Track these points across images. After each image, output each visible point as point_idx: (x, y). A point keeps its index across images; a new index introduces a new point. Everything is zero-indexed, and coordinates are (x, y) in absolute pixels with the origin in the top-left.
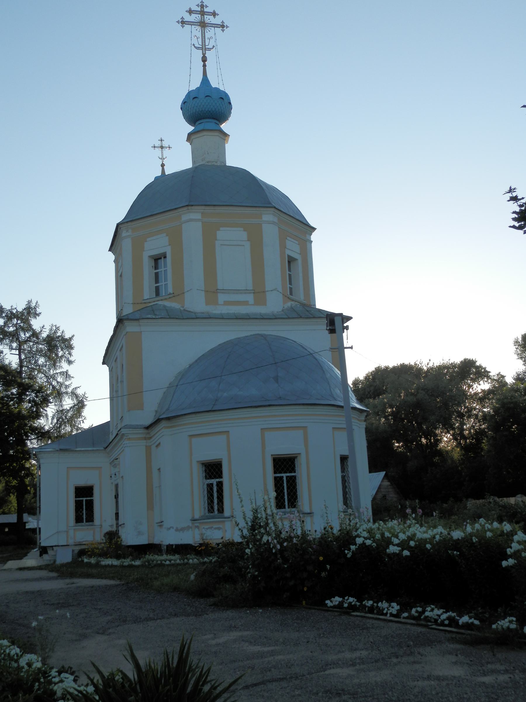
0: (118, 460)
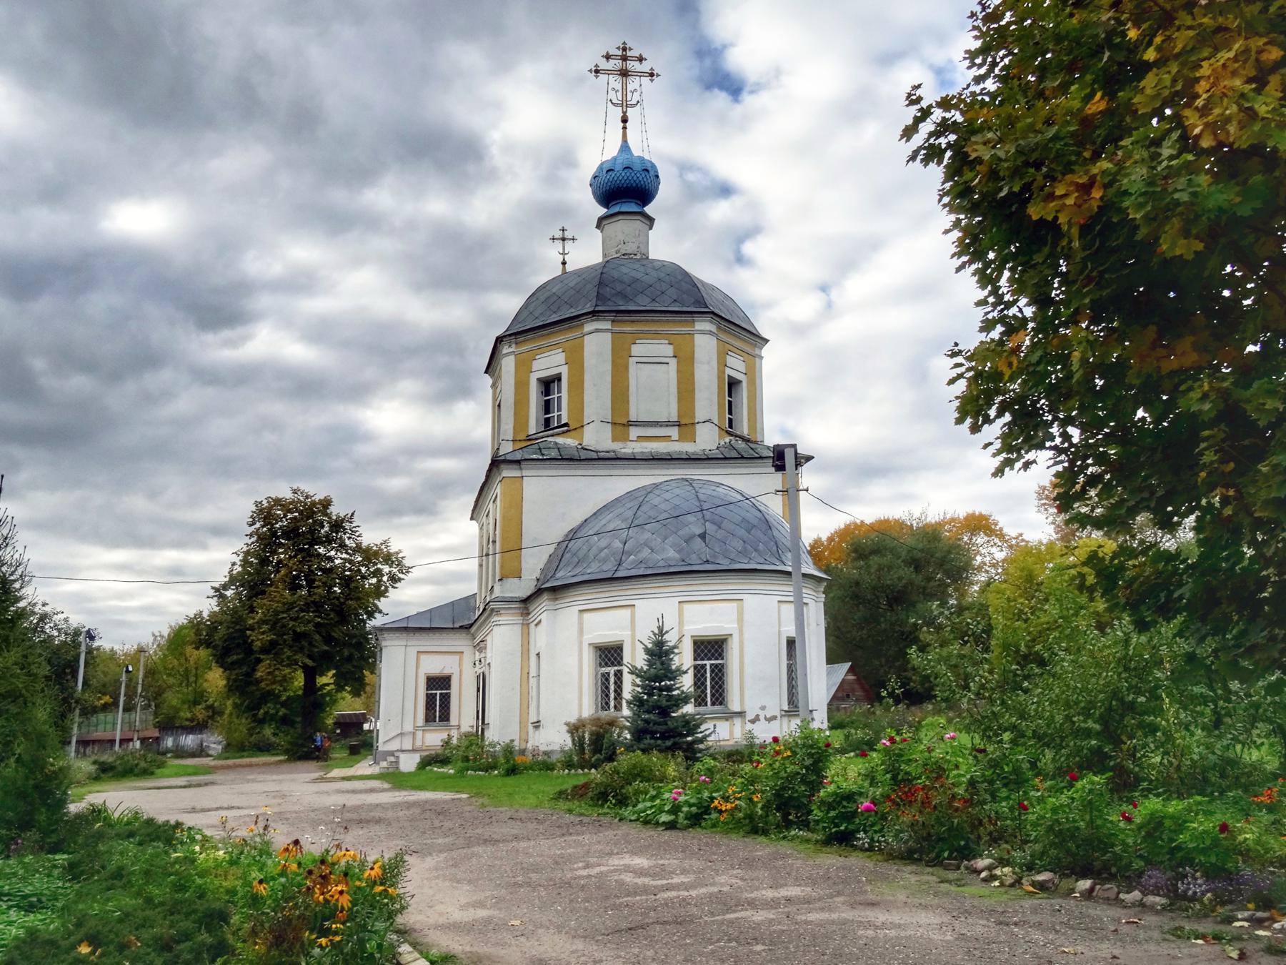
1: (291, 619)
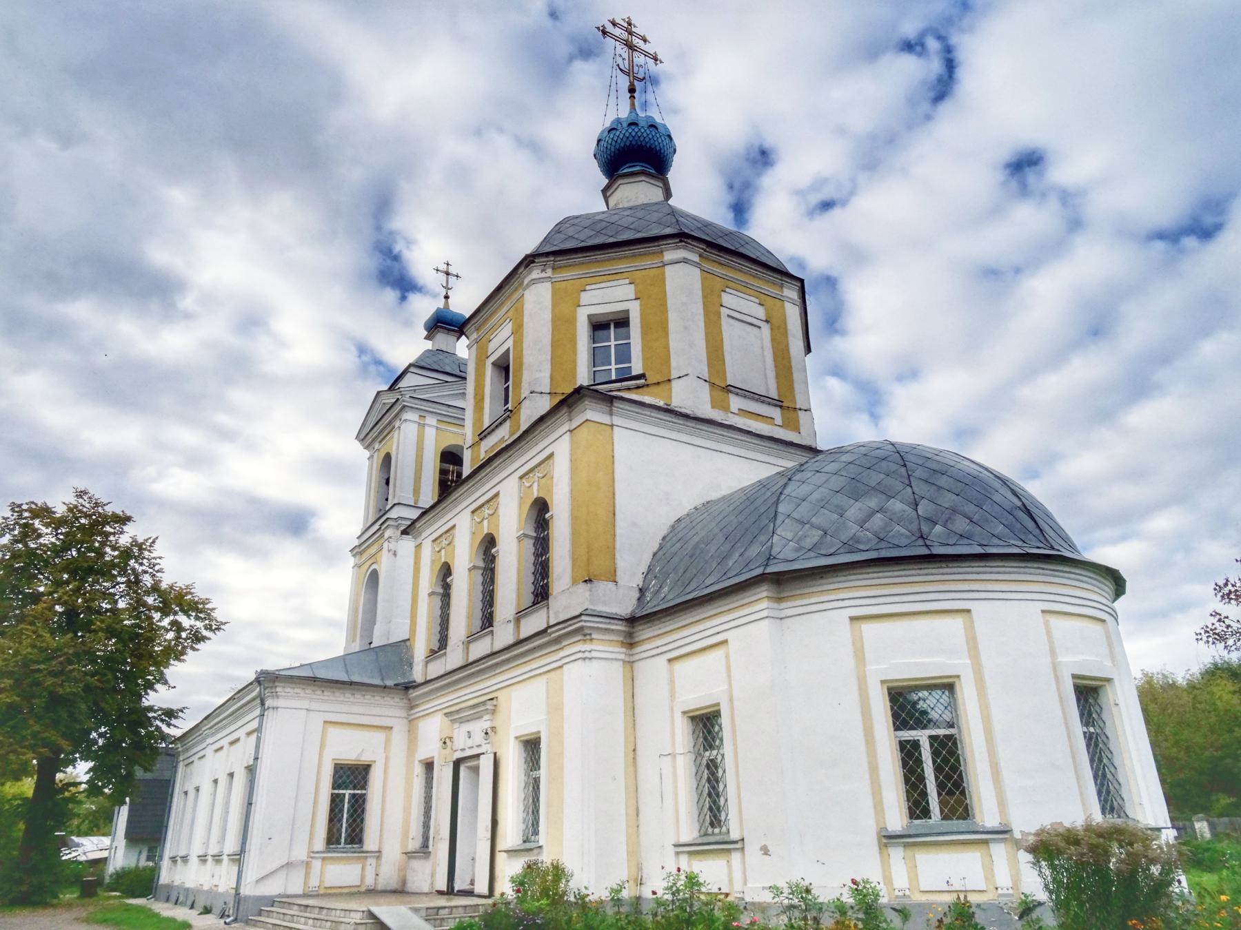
0: (494, 702)
1: (53, 674)
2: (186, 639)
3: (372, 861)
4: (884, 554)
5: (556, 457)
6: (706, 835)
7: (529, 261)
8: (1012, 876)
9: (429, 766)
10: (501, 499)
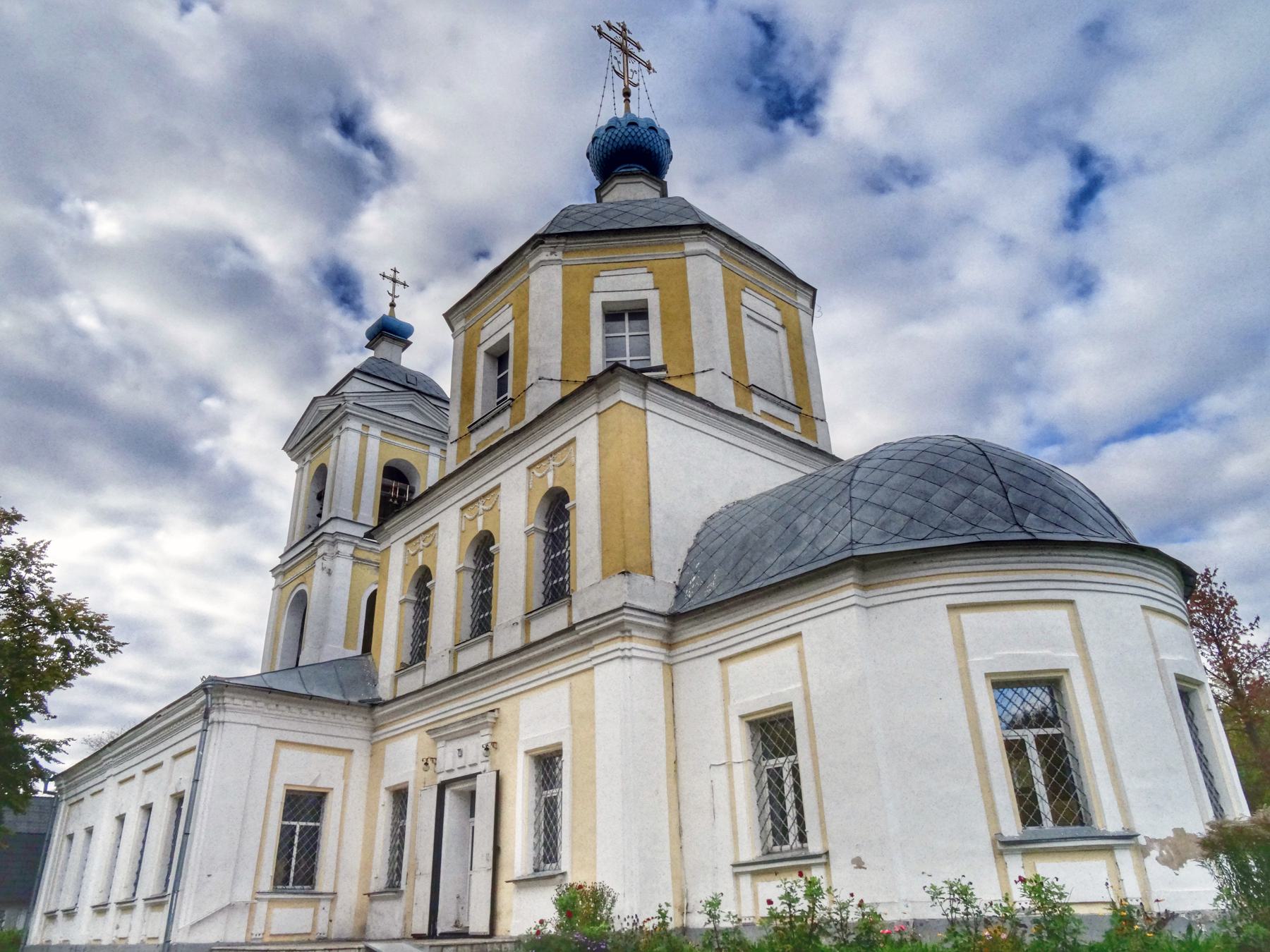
0: (496, 714)
2: (75, 660)
3: (325, 904)
4: (984, 538)
5: (579, 443)
6: (769, 853)
7: (537, 241)
8: (1141, 887)
9: (400, 795)
10: (503, 492)
